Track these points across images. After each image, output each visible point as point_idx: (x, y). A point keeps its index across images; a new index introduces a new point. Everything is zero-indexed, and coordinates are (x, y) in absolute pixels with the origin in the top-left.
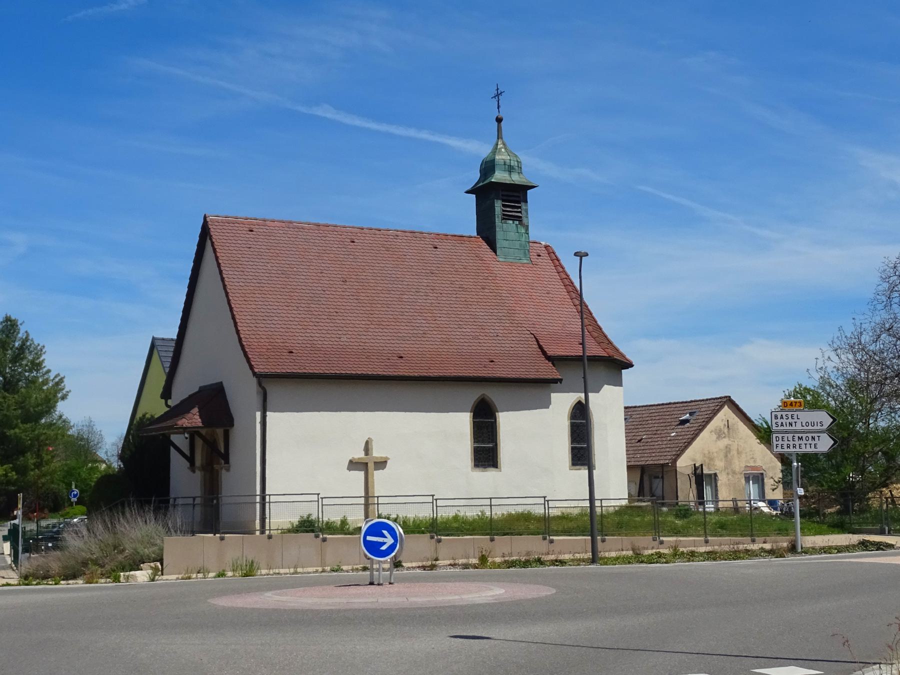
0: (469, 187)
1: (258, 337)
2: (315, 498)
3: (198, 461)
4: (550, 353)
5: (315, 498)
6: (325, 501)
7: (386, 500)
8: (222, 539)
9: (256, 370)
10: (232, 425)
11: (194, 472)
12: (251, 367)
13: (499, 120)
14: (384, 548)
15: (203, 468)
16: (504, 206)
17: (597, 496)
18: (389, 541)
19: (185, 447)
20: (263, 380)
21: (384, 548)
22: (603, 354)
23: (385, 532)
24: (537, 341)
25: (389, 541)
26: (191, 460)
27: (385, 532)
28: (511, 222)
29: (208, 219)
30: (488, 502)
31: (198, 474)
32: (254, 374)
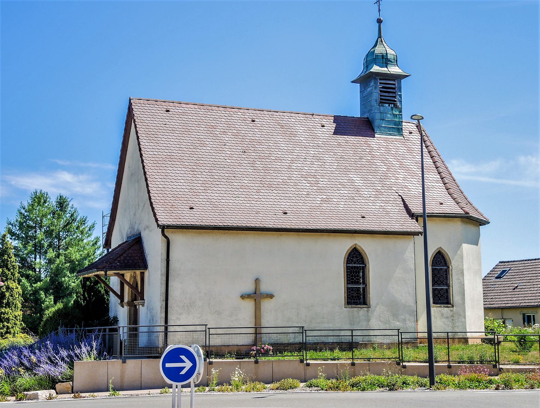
0: (355, 78)
1: (165, 196)
2: (203, 328)
3: (126, 300)
4: (413, 211)
5: (203, 328)
6: (212, 331)
7: (497, 348)
8: (256, 362)
9: (159, 223)
10: (146, 267)
11: (123, 306)
12: (157, 220)
13: (379, 21)
14: (183, 372)
15: (129, 304)
16: (381, 91)
17: (434, 329)
18: (188, 364)
19: (117, 289)
20: (167, 232)
21: (183, 372)
22: (458, 210)
23: (183, 357)
24: (403, 200)
25: (188, 364)
26: (121, 297)
27: (183, 357)
28: (387, 105)
29: (132, 101)
30: (349, 333)
31: (126, 308)
32: (158, 225)
